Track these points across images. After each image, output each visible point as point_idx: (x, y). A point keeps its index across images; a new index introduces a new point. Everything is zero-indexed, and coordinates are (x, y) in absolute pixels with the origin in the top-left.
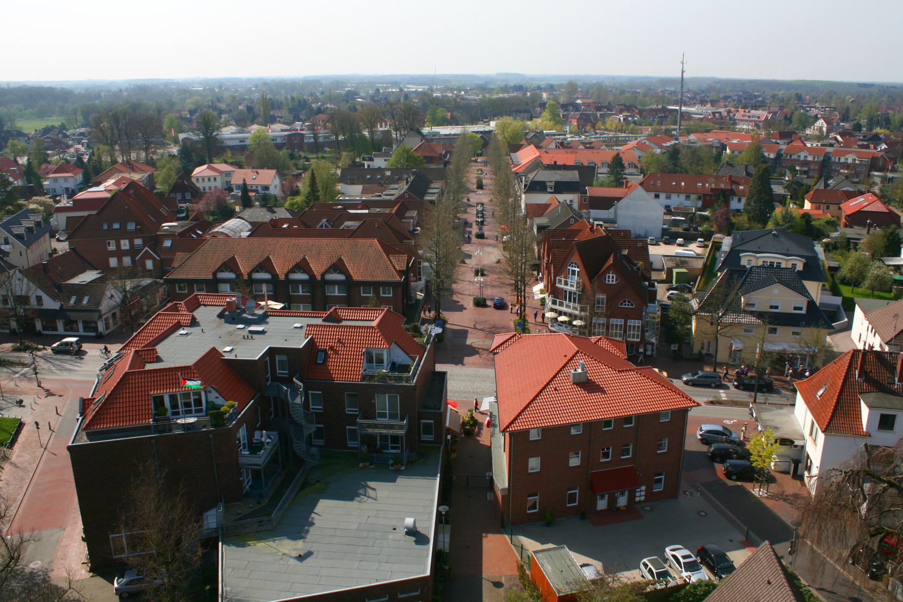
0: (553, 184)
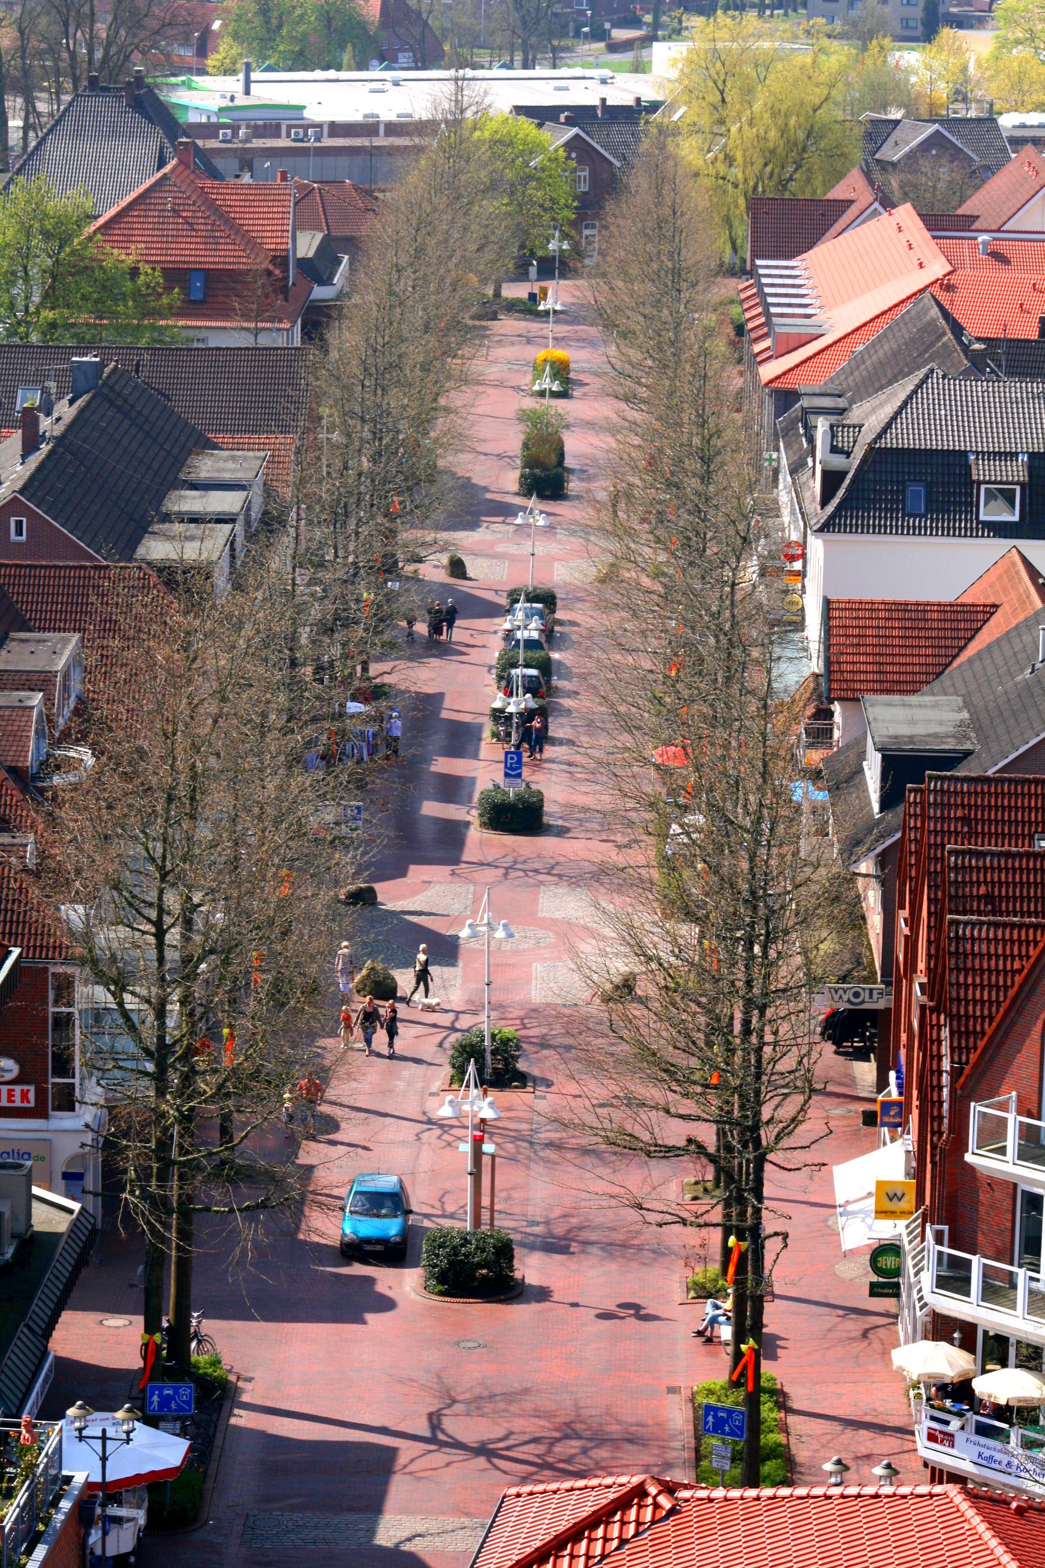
0: (1017, 471)
